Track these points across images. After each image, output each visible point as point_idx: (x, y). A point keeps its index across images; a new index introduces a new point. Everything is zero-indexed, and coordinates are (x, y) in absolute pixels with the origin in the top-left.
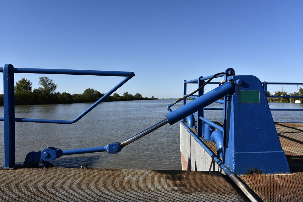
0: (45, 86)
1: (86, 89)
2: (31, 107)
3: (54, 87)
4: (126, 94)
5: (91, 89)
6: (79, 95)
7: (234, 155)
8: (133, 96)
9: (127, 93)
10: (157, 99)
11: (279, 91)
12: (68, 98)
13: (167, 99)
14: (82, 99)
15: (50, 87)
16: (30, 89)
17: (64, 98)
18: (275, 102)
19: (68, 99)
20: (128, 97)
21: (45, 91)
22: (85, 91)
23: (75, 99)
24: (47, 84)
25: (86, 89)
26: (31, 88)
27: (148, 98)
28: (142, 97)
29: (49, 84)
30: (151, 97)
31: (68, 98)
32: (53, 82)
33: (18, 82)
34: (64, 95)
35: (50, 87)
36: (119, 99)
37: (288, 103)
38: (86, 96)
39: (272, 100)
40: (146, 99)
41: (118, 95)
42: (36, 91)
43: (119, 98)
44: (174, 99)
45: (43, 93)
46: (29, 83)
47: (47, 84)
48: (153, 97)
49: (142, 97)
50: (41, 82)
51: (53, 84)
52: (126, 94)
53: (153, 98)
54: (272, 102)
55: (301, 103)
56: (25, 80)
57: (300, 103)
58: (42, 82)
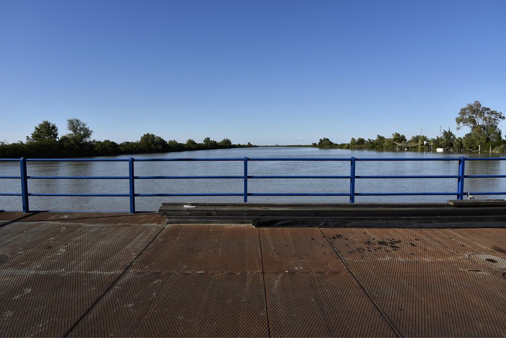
0: (75, 132)
1: (353, 139)
2: (494, 163)
3: (87, 133)
4: (207, 140)
5: (150, 134)
6: (132, 143)
7: (253, 225)
8: (102, 142)
9: (208, 139)
10: (256, 146)
11: (418, 135)
12: (111, 148)
13: (271, 146)
14: (136, 148)
15: (82, 133)
16: (55, 136)
17: (104, 148)
18: (411, 151)
19: (110, 150)
20: (210, 145)
21: (75, 140)
22: (142, 138)
23: (124, 150)
24: (79, 128)
25: (353, 139)
26: (57, 135)
27: (119, 142)
28: (232, 144)
29: (81, 129)
30: (246, 144)
31: (111, 148)
32: (87, 126)
33: (38, 127)
34: (105, 144)
35: (82, 133)
36: (194, 148)
37: (429, 151)
38: (141, 144)
39: (408, 148)
40: (239, 146)
41: (194, 142)
42: (64, 139)
43: (194, 146)
44: (279, 146)
45: (72, 142)
46: (54, 127)
47: (79, 128)
48: (249, 143)
49: (232, 144)
50: (69, 126)
51: (86, 129)
52: (207, 140)
53: (250, 146)
54: (407, 151)
55: (444, 152)
56: (48, 124)
57: (442, 151)
58: (71, 126)
